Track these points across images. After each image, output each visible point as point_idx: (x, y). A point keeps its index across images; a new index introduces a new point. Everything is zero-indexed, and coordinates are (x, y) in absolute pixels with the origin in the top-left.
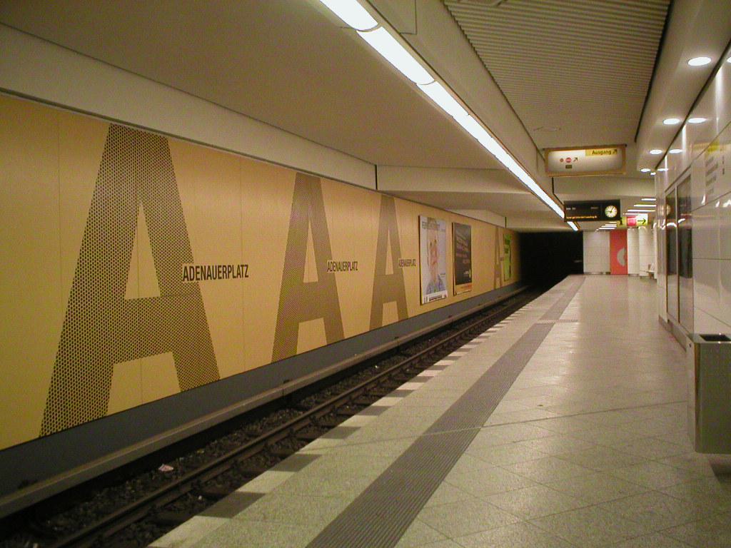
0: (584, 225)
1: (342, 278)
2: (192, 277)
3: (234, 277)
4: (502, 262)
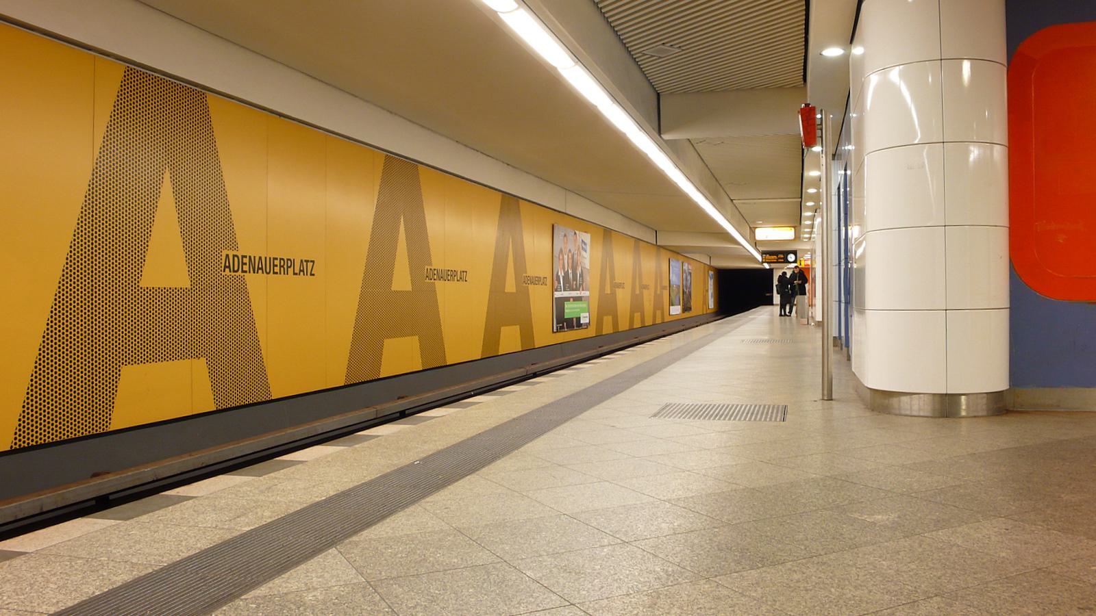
0: (773, 265)
1: (645, 292)
2: (236, 269)
3: (295, 274)
4: (645, 292)
